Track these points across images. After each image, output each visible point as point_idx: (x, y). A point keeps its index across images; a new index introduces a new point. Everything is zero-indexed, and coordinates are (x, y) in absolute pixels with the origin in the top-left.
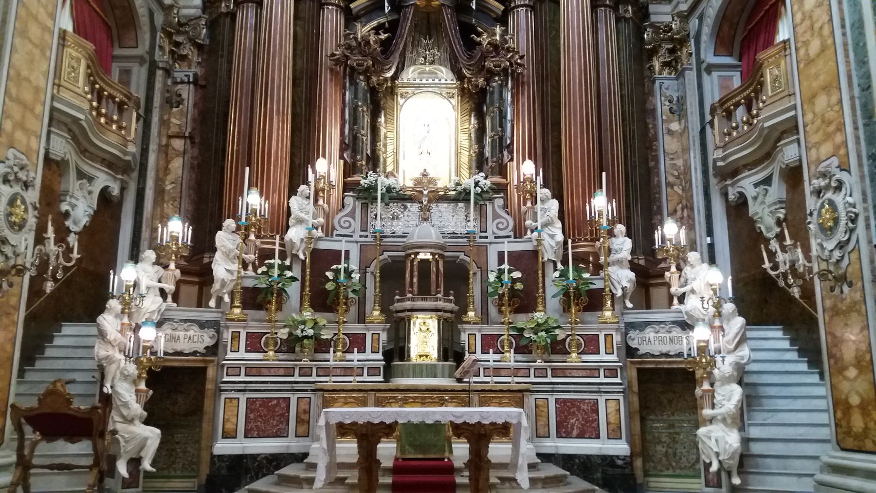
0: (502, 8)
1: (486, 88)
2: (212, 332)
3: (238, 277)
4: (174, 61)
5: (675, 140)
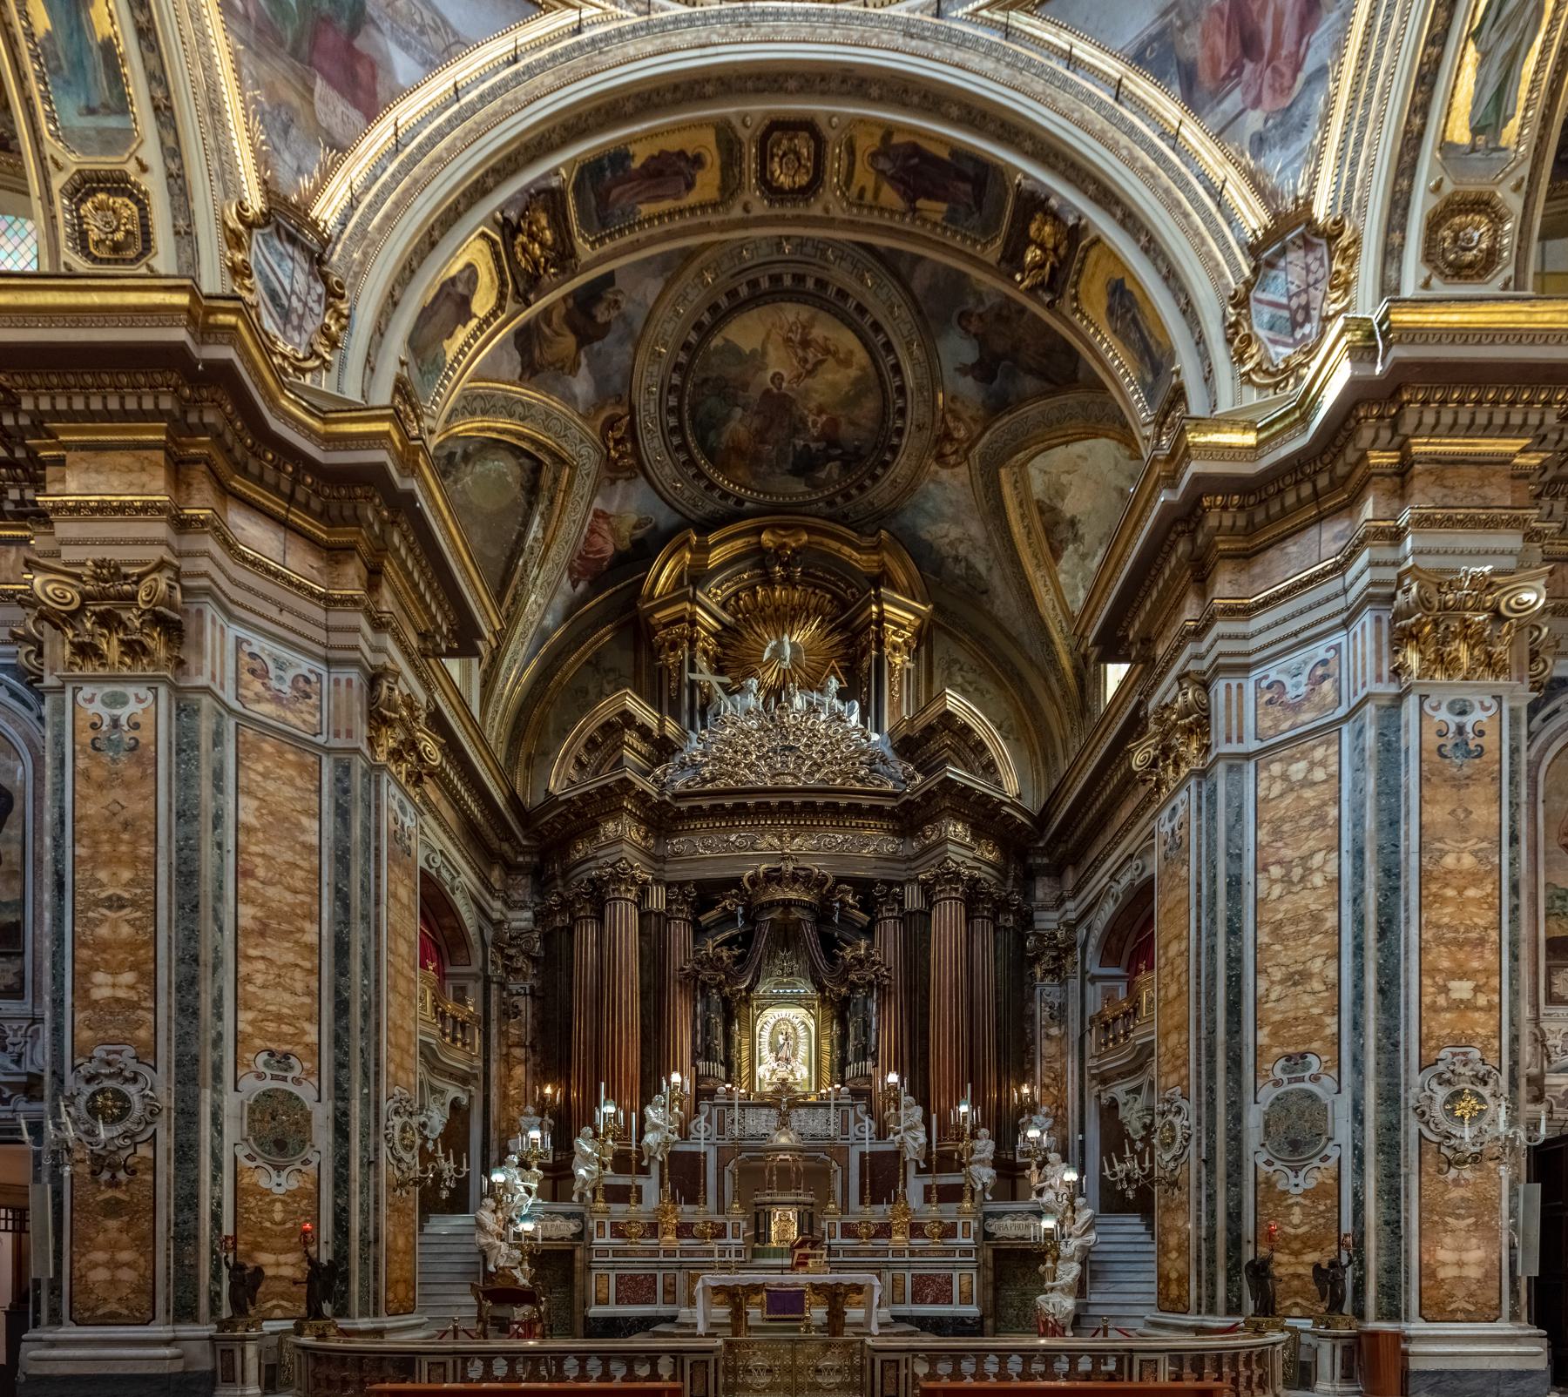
2: (577, 1222)
4: (508, 974)
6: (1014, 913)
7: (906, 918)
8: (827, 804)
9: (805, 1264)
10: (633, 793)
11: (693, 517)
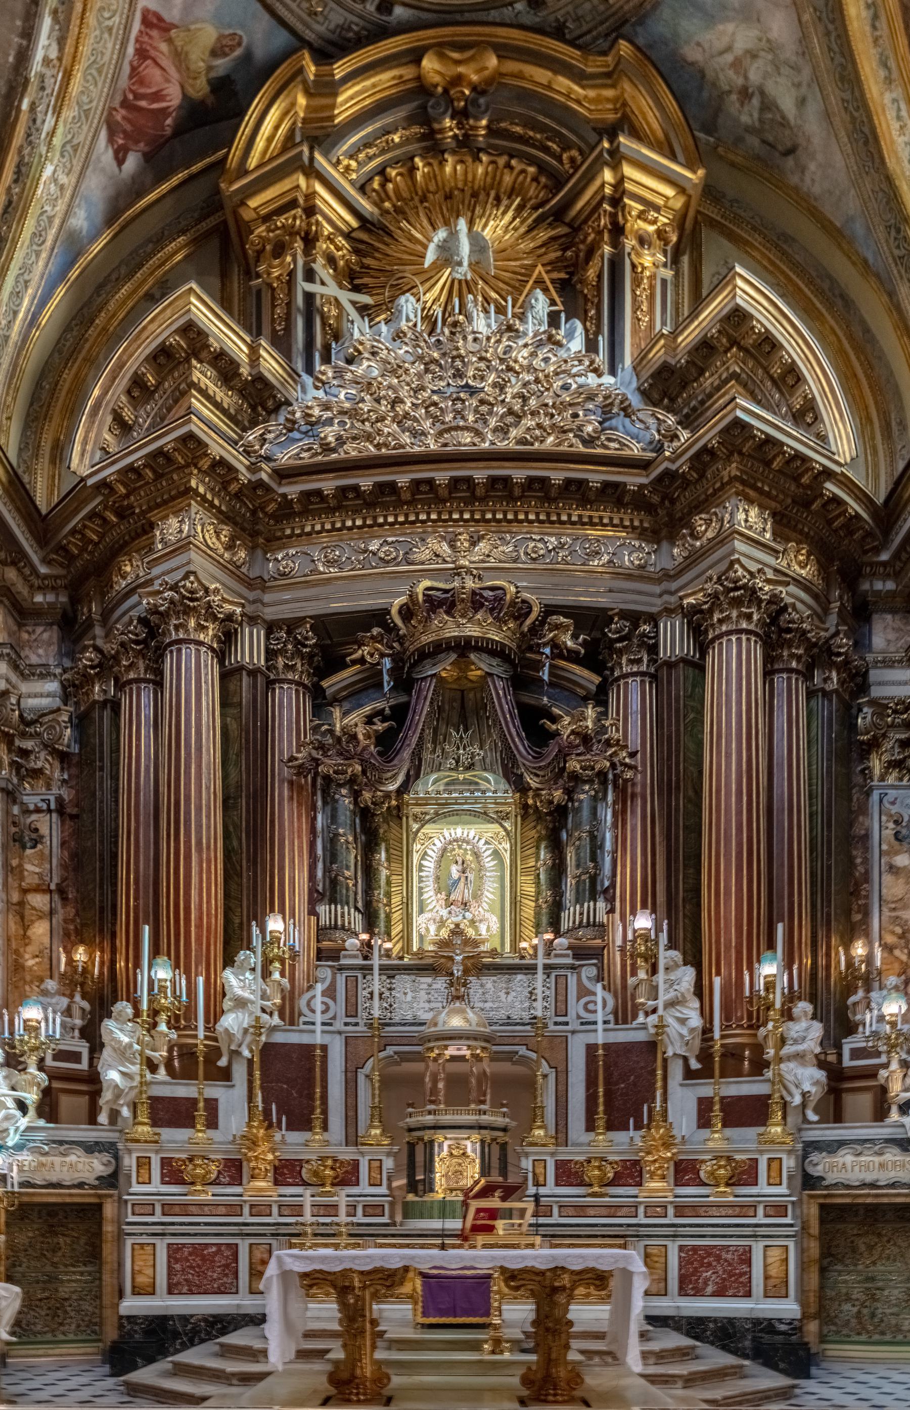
0: (597, 679)
1: (566, 805)
2: (106, 1157)
3: (141, 1083)
4: (22, 779)
5: (901, 881)
6: (840, 668)
8: (531, 480)
9: (490, 1229)
10: (205, 464)
11: (309, 35)
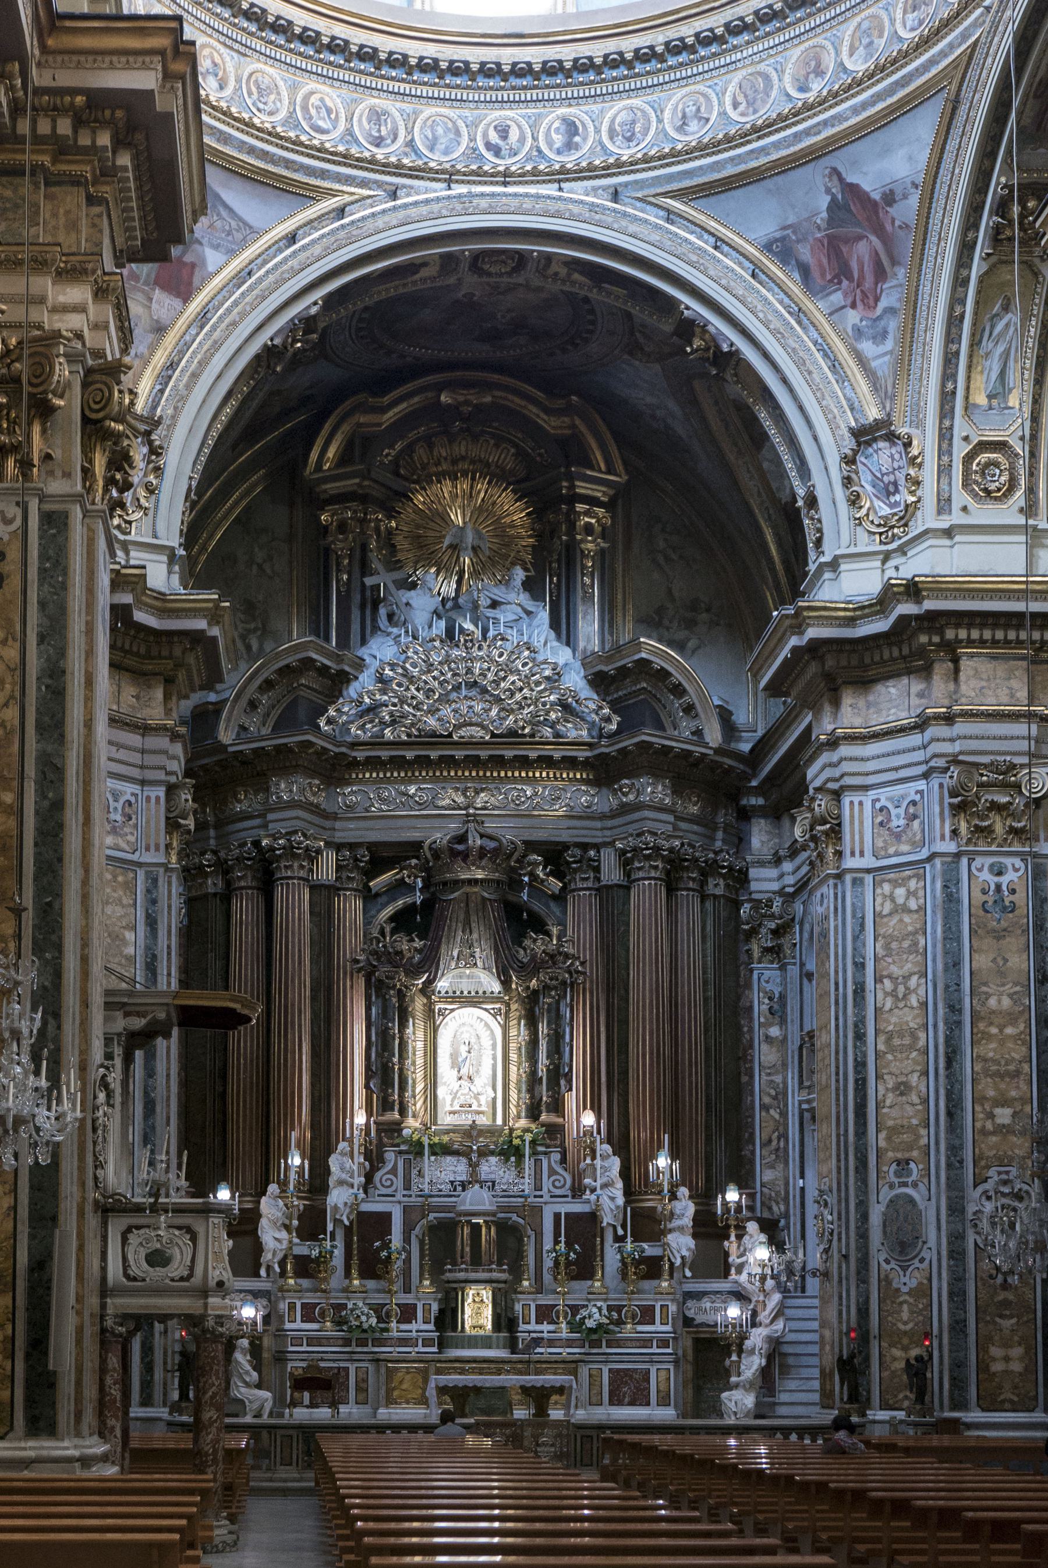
5: (774, 1049)
7: (603, 891)
